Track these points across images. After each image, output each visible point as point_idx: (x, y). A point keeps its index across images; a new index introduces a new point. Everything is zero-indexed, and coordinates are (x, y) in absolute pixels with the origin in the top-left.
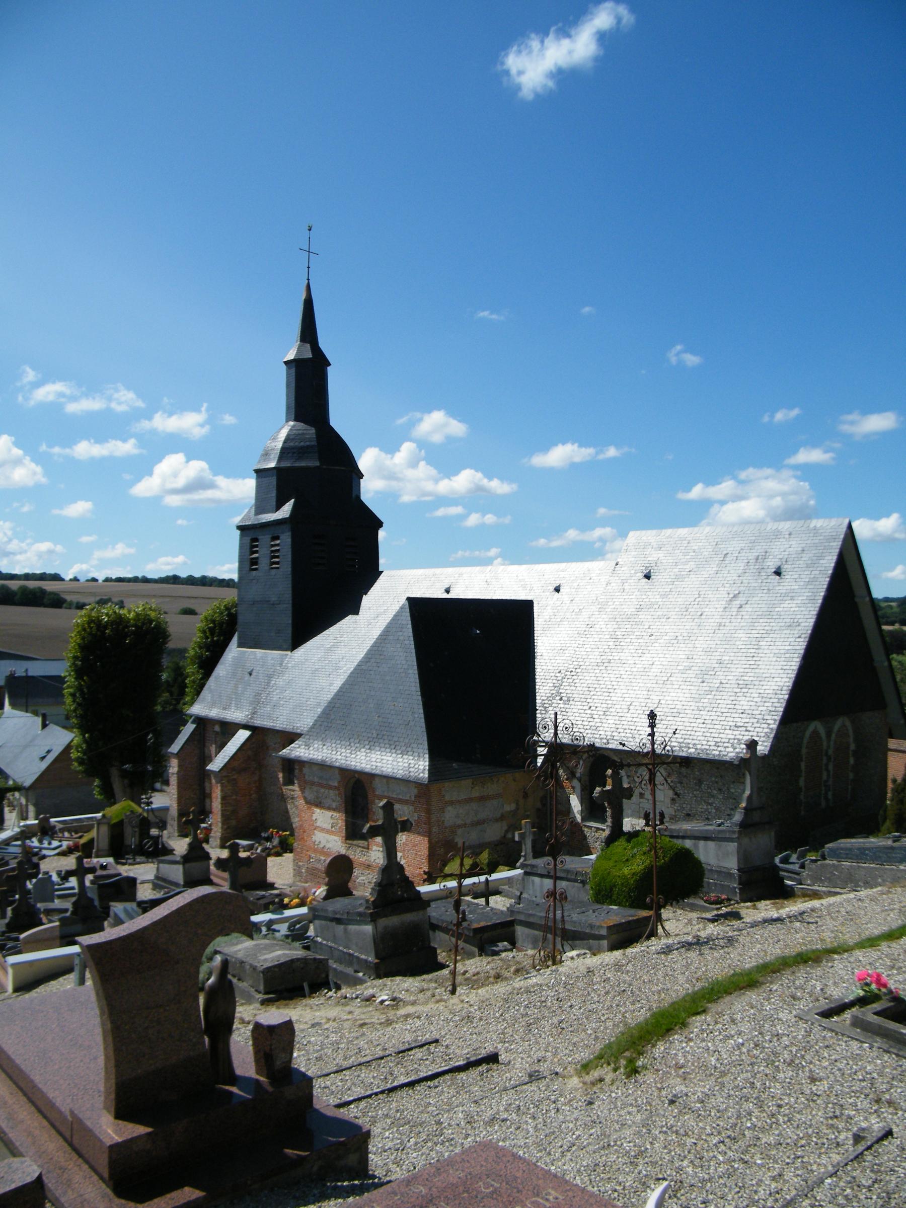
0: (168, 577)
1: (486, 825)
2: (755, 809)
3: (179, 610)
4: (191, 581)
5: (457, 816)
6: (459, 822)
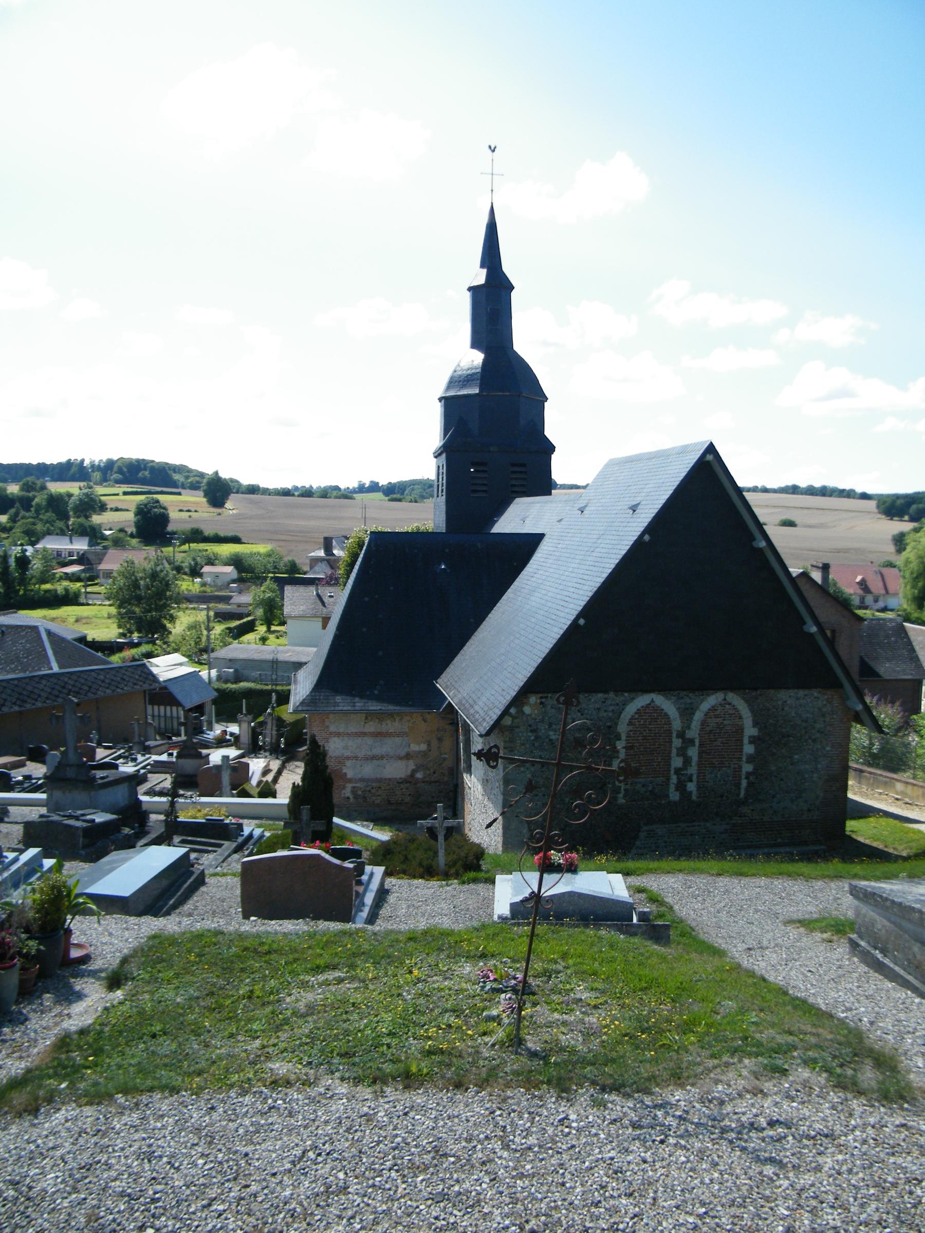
0: (787, 487)
1: (385, 761)
2: (70, 766)
3: (777, 522)
4: (811, 491)
5: (346, 748)
6: (348, 753)
